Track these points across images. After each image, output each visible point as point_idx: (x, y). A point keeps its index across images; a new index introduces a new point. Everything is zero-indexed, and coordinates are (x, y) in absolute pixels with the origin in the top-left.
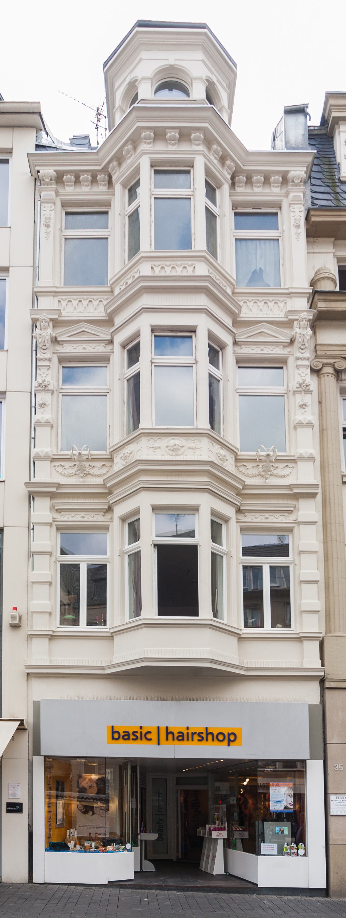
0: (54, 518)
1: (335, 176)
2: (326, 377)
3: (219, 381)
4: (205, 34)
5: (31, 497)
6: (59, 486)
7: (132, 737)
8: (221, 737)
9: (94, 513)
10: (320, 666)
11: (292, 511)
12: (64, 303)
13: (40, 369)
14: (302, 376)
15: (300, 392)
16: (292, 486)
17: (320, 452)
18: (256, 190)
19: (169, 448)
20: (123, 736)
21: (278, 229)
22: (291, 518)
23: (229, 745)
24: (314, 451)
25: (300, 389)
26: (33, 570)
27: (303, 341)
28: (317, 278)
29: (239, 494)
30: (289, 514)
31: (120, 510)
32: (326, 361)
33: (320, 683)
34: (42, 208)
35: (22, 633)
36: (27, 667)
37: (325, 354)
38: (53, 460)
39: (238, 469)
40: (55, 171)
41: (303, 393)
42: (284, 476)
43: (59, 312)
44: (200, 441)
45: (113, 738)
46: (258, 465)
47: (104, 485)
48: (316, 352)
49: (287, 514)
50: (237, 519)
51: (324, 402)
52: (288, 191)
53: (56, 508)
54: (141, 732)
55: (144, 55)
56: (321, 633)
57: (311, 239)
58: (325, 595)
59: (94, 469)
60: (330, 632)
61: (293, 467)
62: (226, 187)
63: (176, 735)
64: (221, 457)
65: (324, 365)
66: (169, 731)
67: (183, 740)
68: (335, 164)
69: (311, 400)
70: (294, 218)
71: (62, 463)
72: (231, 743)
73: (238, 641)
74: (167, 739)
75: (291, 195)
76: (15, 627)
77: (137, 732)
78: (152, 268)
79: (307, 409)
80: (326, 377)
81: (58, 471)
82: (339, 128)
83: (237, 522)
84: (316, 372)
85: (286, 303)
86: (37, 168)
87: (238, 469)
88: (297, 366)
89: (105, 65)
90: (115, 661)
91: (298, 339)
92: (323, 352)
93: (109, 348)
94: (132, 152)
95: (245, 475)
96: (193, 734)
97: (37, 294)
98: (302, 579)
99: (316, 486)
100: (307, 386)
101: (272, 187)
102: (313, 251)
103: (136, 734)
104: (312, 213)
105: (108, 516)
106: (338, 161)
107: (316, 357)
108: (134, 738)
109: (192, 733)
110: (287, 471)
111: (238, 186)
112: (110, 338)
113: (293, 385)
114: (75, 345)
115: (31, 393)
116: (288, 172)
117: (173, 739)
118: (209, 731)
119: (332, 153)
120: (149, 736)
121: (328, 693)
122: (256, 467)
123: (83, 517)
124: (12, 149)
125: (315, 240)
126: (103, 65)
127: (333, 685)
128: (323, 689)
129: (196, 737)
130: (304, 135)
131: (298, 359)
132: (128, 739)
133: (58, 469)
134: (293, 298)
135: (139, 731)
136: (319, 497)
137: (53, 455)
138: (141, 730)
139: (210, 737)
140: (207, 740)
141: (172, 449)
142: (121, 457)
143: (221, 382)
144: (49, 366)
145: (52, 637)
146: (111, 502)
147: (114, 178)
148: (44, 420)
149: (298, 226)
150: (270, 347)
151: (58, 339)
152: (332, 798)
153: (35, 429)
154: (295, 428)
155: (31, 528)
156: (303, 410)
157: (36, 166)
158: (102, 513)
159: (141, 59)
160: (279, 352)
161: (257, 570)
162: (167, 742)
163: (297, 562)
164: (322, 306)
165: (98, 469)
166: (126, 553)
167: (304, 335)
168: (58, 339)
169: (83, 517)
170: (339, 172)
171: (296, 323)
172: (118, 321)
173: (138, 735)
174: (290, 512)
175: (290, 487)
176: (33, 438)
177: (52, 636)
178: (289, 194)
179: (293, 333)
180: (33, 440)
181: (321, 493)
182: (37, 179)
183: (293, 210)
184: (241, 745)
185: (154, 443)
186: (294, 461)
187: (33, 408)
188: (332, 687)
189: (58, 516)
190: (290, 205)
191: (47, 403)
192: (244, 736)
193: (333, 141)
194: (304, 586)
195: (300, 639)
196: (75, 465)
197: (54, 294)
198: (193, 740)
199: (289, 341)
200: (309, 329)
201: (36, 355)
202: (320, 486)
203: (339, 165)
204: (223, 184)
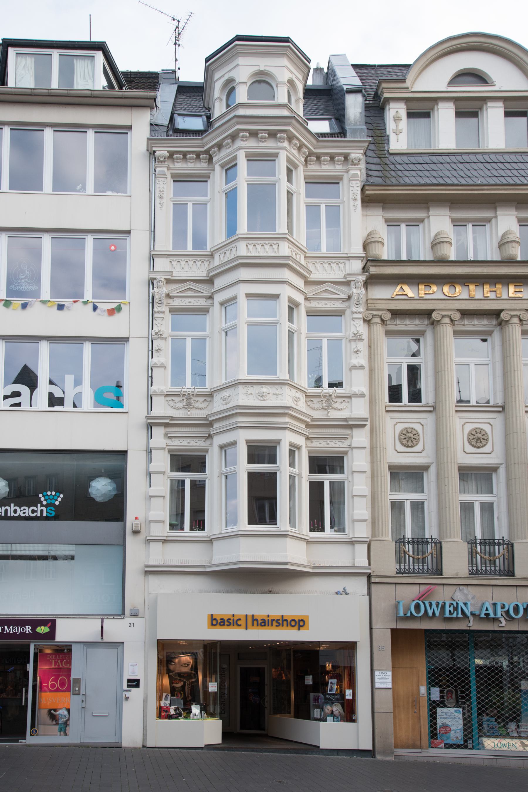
0: (166, 444)
1: (385, 147)
2: (375, 326)
3: (294, 333)
4: (289, 47)
5: (149, 427)
6: (172, 418)
7: (226, 623)
8: (293, 623)
9: (198, 440)
10: (368, 566)
11: (347, 438)
12: (174, 263)
13: (156, 320)
14: (356, 327)
15: (355, 340)
16: (348, 419)
17: (369, 388)
18: (324, 167)
19: (259, 394)
20: (221, 622)
21: (339, 198)
22: (346, 443)
23: (299, 629)
24: (365, 390)
25: (355, 338)
26: (150, 486)
27: (358, 299)
28: (369, 241)
29: (308, 426)
30: (345, 440)
31: (219, 440)
32: (375, 313)
33: (367, 577)
34: (157, 181)
35: (141, 537)
36: (146, 566)
37: (375, 307)
38: (167, 395)
39: (307, 404)
40: (168, 151)
41: (357, 341)
42: (342, 409)
43: (172, 273)
44: (281, 388)
45: (213, 625)
46: (322, 401)
47: (206, 418)
48: (368, 304)
49: (344, 441)
50: (306, 445)
51: (372, 347)
52: (348, 169)
53: (169, 435)
54: (234, 619)
55: (241, 60)
56: (369, 538)
57: (365, 204)
58: (372, 506)
59: (198, 403)
60: (375, 536)
61: (348, 402)
62: (301, 168)
63: (260, 622)
64: (296, 399)
65: (374, 316)
66: (254, 618)
67: (265, 625)
68: (386, 136)
69: (363, 346)
70: (352, 192)
71: (173, 398)
72: (301, 628)
73: (306, 543)
74: (253, 625)
75: (352, 172)
76: (136, 533)
77: (230, 619)
78: (247, 245)
79: (360, 354)
80: (375, 326)
81: (170, 405)
82: (389, 104)
83: (306, 447)
84: (367, 321)
85: (345, 264)
86: (154, 149)
87: (307, 404)
88: (353, 318)
89: (207, 60)
90: (214, 562)
91: (355, 297)
92: (373, 305)
93: (210, 302)
94: (231, 144)
95: (312, 409)
96: (273, 620)
97: (154, 256)
98: (354, 494)
99: (366, 419)
100: (360, 335)
101: (336, 165)
102: (366, 214)
103: (229, 621)
104: (367, 188)
105: (208, 442)
106: (388, 133)
107: (367, 309)
108: (228, 624)
109: (272, 620)
110: (344, 405)
111: (309, 164)
112: (210, 295)
113: (350, 334)
114: (183, 300)
115: (148, 338)
116: (348, 154)
117: (258, 625)
118: (284, 618)
119: (382, 125)
120: (239, 623)
121: (373, 587)
122: (320, 401)
123: (189, 443)
124: (131, 126)
125: (368, 205)
126: (206, 59)
127: (377, 580)
128: (370, 583)
129: (275, 623)
130: (361, 113)
131: (353, 313)
132: (224, 625)
133: (170, 403)
134: (351, 261)
135: (232, 618)
136: (368, 427)
137: (167, 392)
138: (233, 618)
139: (285, 623)
140: (283, 626)
141: (261, 395)
142: (221, 398)
143: (295, 334)
144: (163, 318)
145: (165, 541)
146: (212, 433)
147: (215, 159)
148: (160, 363)
149: (355, 200)
150: (332, 302)
151: (170, 295)
152: (377, 673)
153: (152, 370)
154: (350, 370)
155: (149, 452)
156: (357, 355)
157: (153, 147)
158: (204, 440)
159: (238, 65)
160: (339, 306)
161: (321, 485)
162: (253, 627)
163: (350, 479)
164: (373, 270)
165: (200, 403)
166: (223, 474)
167: (358, 294)
168: (170, 295)
169: (189, 443)
170: (388, 144)
171: (352, 283)
172: (219, 283)
173: (231, 621)
174: (346, 439)
175: (346, 420)
176: (150, 377)
177: (165, 540)
178: (349, 171)
179: (350, 292)
180: (150, 379)
181: (369, 448)
182: (152, 154)
183: (352, 185)
184: (308, 629)
185: (247, 390)
186: (350, 397)
187: (151, 352)
188: (376, 582)
189: (169, 442)
190: (350, 181)
191: (162, 349)
192: (311, 623)
193: (384, 112)
194: (356, 499)
195: (352, 543)
196: (183, 400)
197: (167, 256)
198: (272, 625)
199: (347, 297)
200: (363, 289)
201: (153, 308)
202: (369, 420)
203: (388, 136)
204: (299, 166)
